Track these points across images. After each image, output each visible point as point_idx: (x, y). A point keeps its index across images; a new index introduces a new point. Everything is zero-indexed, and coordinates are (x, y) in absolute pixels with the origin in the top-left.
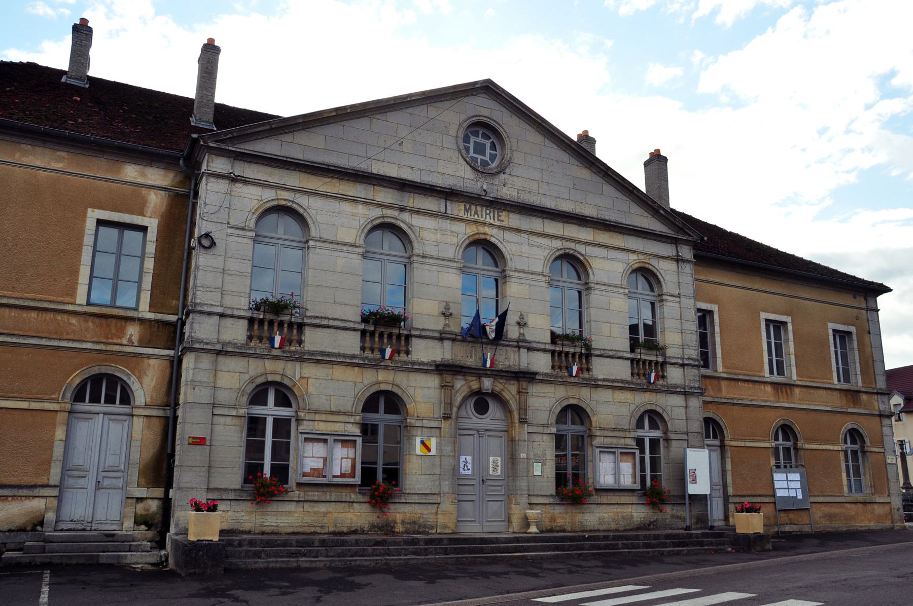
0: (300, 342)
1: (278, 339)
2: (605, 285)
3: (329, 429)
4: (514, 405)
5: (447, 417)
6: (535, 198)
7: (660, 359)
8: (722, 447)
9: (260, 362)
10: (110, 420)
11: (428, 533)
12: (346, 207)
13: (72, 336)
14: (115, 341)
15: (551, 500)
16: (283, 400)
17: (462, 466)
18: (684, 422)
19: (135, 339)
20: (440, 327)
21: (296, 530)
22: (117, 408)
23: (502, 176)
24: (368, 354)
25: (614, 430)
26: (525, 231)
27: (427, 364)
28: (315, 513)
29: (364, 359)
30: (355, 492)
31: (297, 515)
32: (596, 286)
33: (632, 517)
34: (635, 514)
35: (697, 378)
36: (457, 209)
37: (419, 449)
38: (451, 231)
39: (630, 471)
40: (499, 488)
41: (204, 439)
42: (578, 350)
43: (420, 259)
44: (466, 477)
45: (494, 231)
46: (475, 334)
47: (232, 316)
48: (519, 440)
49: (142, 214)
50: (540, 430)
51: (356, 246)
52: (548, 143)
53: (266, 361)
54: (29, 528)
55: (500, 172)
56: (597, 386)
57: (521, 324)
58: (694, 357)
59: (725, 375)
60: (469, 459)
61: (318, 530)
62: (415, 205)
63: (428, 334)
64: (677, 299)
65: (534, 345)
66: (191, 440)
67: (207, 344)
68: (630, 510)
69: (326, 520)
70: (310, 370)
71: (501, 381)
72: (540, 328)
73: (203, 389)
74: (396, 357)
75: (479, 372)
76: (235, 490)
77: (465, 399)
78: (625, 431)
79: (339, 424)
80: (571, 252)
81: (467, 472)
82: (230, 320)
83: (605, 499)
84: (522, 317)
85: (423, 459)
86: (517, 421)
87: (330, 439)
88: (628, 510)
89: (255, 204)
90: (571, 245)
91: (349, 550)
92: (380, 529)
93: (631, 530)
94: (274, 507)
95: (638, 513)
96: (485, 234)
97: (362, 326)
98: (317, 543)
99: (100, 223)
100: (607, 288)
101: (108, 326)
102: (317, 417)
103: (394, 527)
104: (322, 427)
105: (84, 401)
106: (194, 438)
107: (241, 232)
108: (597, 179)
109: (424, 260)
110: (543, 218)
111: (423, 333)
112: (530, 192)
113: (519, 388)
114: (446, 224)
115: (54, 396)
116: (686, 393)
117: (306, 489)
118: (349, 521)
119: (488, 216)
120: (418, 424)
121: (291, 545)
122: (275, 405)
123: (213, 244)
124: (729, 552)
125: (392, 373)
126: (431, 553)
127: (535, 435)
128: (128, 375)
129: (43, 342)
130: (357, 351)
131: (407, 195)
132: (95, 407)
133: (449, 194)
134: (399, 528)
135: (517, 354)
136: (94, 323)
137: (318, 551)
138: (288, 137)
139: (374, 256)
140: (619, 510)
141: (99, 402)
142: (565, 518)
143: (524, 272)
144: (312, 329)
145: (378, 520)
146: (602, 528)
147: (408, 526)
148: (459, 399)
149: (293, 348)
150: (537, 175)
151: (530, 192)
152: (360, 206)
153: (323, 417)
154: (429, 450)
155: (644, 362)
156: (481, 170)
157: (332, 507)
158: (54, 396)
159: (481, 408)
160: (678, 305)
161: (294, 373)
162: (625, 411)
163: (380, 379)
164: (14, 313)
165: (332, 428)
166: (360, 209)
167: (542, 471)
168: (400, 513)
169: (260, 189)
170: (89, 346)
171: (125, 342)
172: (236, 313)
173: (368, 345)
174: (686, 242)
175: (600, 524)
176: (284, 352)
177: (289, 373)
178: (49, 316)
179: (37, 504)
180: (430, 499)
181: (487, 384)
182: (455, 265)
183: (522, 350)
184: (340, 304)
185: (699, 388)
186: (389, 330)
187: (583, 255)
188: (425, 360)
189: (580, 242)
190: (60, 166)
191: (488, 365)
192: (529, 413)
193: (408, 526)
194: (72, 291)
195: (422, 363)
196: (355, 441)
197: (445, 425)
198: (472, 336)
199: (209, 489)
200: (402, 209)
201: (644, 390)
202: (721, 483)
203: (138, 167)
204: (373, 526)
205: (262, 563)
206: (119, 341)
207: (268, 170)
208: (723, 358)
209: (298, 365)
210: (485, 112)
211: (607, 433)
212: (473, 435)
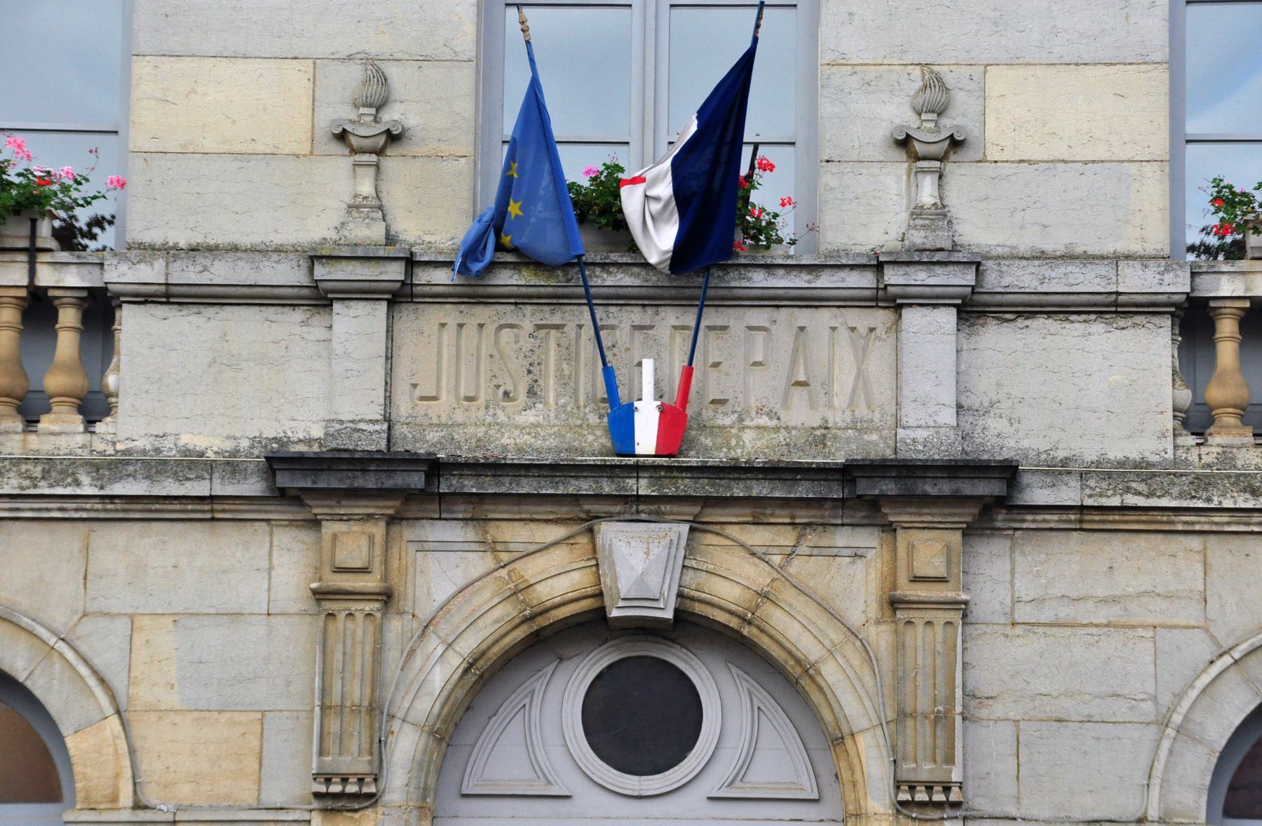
4: (851, 693)
20: (319, 225)
27: (232, 466)
46: (541, 238)
57: (934, 147)
63: (221, 272)
71: (758, 537)
75: (583, 491)
77: (492, 677)
111: (187, 274)
135: (880, 353)
148: (436, 675)
159: (643, 723)
181: (640, 563)
188: (208, 440)
191: (646, 439)
195: (194, 463)
198: (527, 260)
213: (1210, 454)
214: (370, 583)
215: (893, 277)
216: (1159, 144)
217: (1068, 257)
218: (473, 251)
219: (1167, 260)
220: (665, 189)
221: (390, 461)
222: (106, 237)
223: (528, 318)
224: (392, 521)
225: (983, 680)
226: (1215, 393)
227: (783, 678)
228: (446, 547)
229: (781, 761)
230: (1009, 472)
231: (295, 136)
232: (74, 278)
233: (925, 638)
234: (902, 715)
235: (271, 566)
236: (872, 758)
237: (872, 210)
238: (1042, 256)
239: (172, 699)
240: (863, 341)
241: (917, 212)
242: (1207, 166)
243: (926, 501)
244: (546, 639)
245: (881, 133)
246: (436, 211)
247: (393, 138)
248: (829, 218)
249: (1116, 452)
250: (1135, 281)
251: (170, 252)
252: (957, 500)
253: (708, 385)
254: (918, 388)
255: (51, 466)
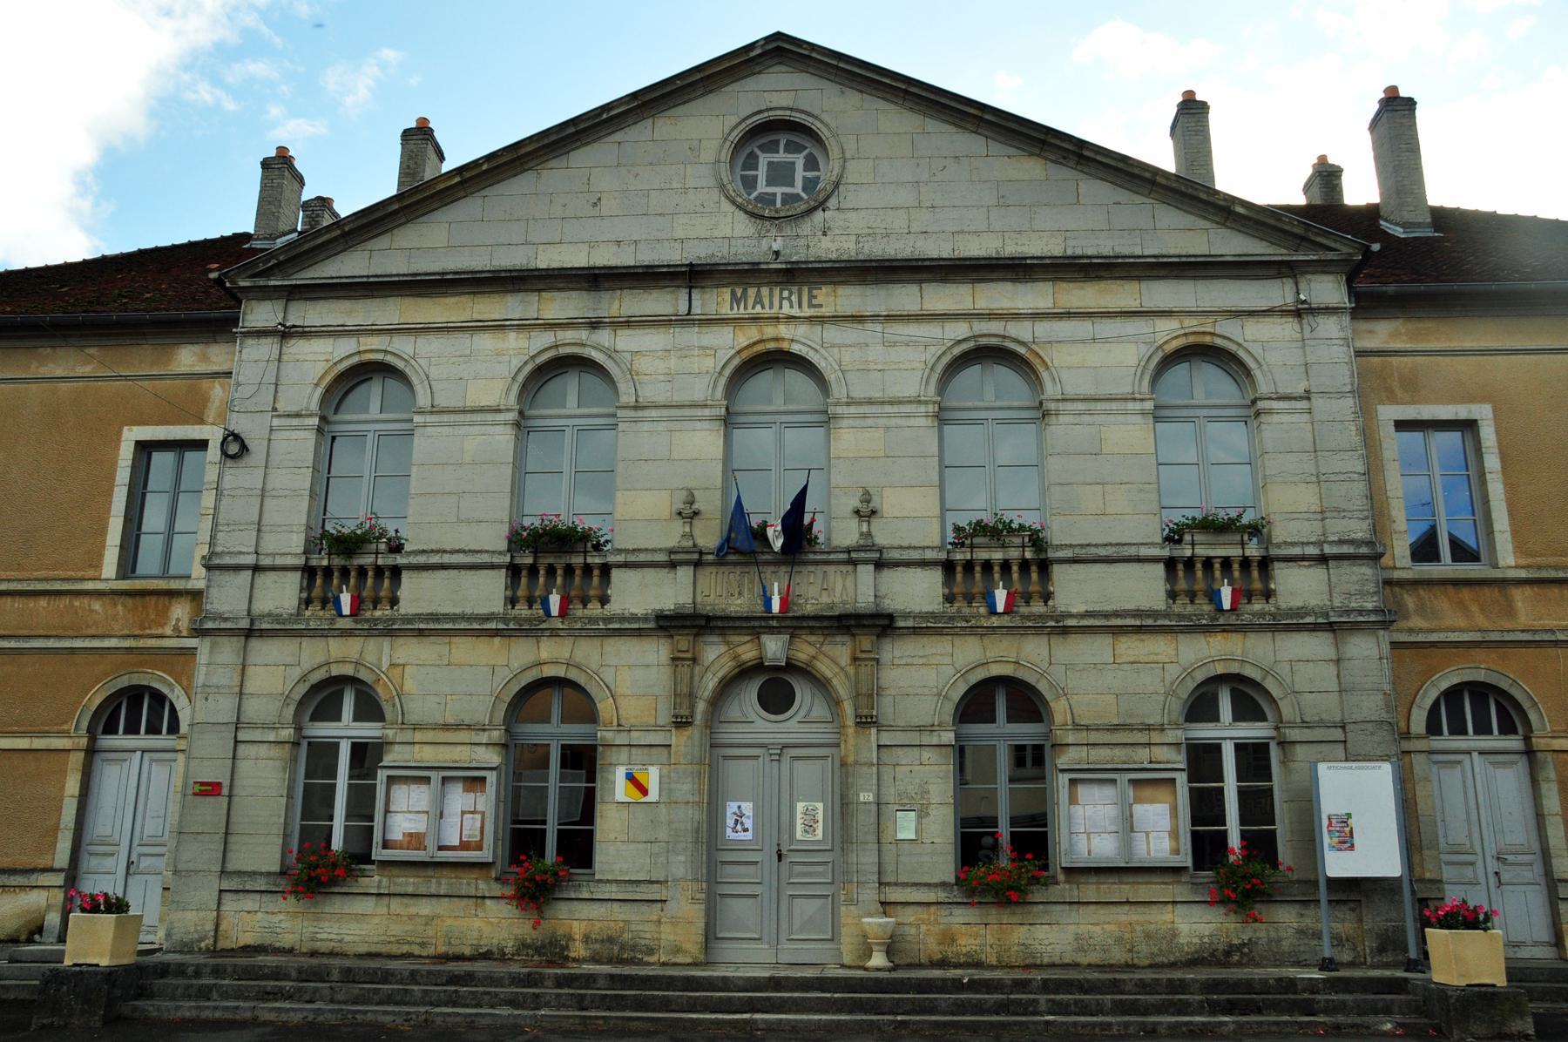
0: (1268, 595)
1: (346, 599)
2: (691, 406)
3: (440, 757)
4: (841, 687)
5: (681, 723)
6: (900, 245)
7: (1253, 550)
8: (1529, 752)
9: (319, 644)
10: (152, 760)
11: (641, 963)
12: (485, 341)
13: (92, 631)
14: (154, 632)
15: (942, 896)
16: (369, 708)
17: (730, 822)
18: (1335, 697)
19: (184, 625)
20: (672, 542)
21: (373, 949)
22: (162, 740)
23: (819, 216)
24: (522, 610)
25: (1115, 728)
26: (875, 317)
27: (645, 619)
28: (411, 917)
29: (505, 620)
30: (487, 879)
31: (376, 920)
32: (1061, 406)
33: (1174, 934)
34: (1184, 928)
35: (1371, 587)
36: (716, 301)
37: (621, 790)
38: (703, 348)
39: (1165, 823)
40: (820, 869)
41: (219, 785)
42: (1014, 554)
43: (632, 413)
44: (741, 847)
45: (801, 331)
46: (741, 545)
47: (274, 568)
48: (856, 763)
49: (201, 421)
50: (913, 738)
51: (499, 411)
52: (932, 125)
53: (331, 640)
54: (23, 937)
55: (815, 209)
56: (1065, 631)
57: (865, 513)
58: (1359, 535)
59: (1523, 574)
60: (747, 808)
61: (416, 950)
62: (614, 311)
63: (642, 557)
64: (1304, 404)
65: (895, 555)
66: (197, 788)
67: (226, 619)
68: (1168, 917)
69: (431, 933)
70: (409, 651)
71: (812, 639)
72: (914, 516)
73: (221, 699)
74: (578, 610)
75: (755, 625)
76: (269, 874)
77: (729, 685)
78: (1148, 728)
79: (460, 748)
80: (994, 341)
81: (742, 836)
82: (271, 576)
83: (1090, 891)
84: (867, 498)
85: (634, 811)
86: (850, 722)
87: (435, 776)
88: (1162, 918)
89: (321, 368)
90: (995, 327)
91: (376, 991)
92: (538, 950)
93: (1172, 965)
94: (336, 905)
95: (1196, 924)
96: (777, 339)
97: (1166, 552)
98: (335, 975)
99: (1401, 425)
100: (1092, 406)
101: (145, 607)
102: (418, 736)
103: (567, 948)
104: (428, 755)
105: (116, 732)
106: (202, 784)
107: (295, 422)
108: (1065, 175)
109: (640, 413)
110: (920, 282)
111: (632, 558)
112: (888, 235)
113: (854, 653)
114: (692, 336)
115: (65, 727)
116: (1334, 626)
117: (395, 871)
118: (475, 934)
119: (786, 302)
120: (621, 739)
121: (287, 977)
122: (355, 720)
123: (244, 448)
124: (1386, 1034)
125: (568, 642)
126: (547, 1005)
127: (900, 751)
128: (170, 685)
129: (51, 643)
130: (498, 606)
131: (605, 296)
132: (1459, 743)
133: (694, 276)
134: (578, 950)
136: (125, 606)
137: (316, 990)
138: (382, 242)
139: (1177, 413)
140: (1134, 918)
141: (138, 733)
142: (977, 934)
143: (870, 402)
144: (415, 574)
145: (535, 934)
146: (1084, 960)
147: (597, 946)
148: (710, 683)
149: (378, 613)
150: (905, 197)
151: (888, 235)
152: (512, 335)
153: (430, 736)
154: (645, 792)
155: (1208, 563)
156: (761, 213)
157: (442, 907)
158: (65, 727)
159: (776, 698)
160: (1306, 417)
161: (380, 659)
162: (1150, 682)
163: (544, 655)
164: (18, 603)
165: (448, 757)
166: (513, 340)
167: (923, 831)
168: (580, 919)
169: (330, 341)
170: (113, 643)
171: (168, 631)
172: (279, 561)
173: (317, 592)
174: (1323, 267)
175: (1081, 949)
176: (356, 622)
177: (370, 658)
178: (65, 602)
179: (34, 900)
180: (643, 893)
181: (774, 647)
182: (707, 412)
183: (860, 568)
184: (468, 521)
185: (1376, 611)
186: (566, 559)
187: (1023, 344)
188: (638, 610)
189: (1016, 316)
190: (87, 370)
191: (776, 607)
192: (886, 702)
193: (597, 946)
194: (96, 561)
195: (634, 618)
196: (484, 779)
197: (678, 739)
198: (737, 552)
199: (223, 873)
200: (595, 325)
201: (1208, 629)
202: (1536, 846)
203: (196, 348)
204: (523, 946)
205: (190, 1008)
206: (160, 631)
207: (346, 305)
208: (1515, 532)
209: (386, 642)
210: (784, 100)
211: (1094, 737)
212: (756, 757)
213: (954, 609)
214: (689, 655)
215: (854, 555)
216: (937, 512)
217: (909, 548)
218: (720, 549)
219: (941, 548)
220: (779, 528)
221: (695, 616)
222: (609, 546)
223: (738, 570)
224: (696, 635)
225: (883, 683)
226: (955, 590)
227: (821, 684)
228: (713, 643)
229: (820, 711)
230: (891, 617)
231: (665, 514)
232: (597, 560)
233: (865, 670)
234: (858, 695)
235: (656, 652)
236: (848, 708)
237: (846, 533)
238: (901, 547)
239: (628, 692)
240: (844, 575)
241: (862, 534)
242: (952, 519)
243: (864, 626)
244: (744, 673)
245: (850, 508)
246: (709, 536)
247: (696, 513)
248: (834, 536)
249: (925, 609)
250: (930, 555)
251: (626, 551)
252: (874, 626)
253: (796, 590)
254: (859, 590)
255: (592, 620)
